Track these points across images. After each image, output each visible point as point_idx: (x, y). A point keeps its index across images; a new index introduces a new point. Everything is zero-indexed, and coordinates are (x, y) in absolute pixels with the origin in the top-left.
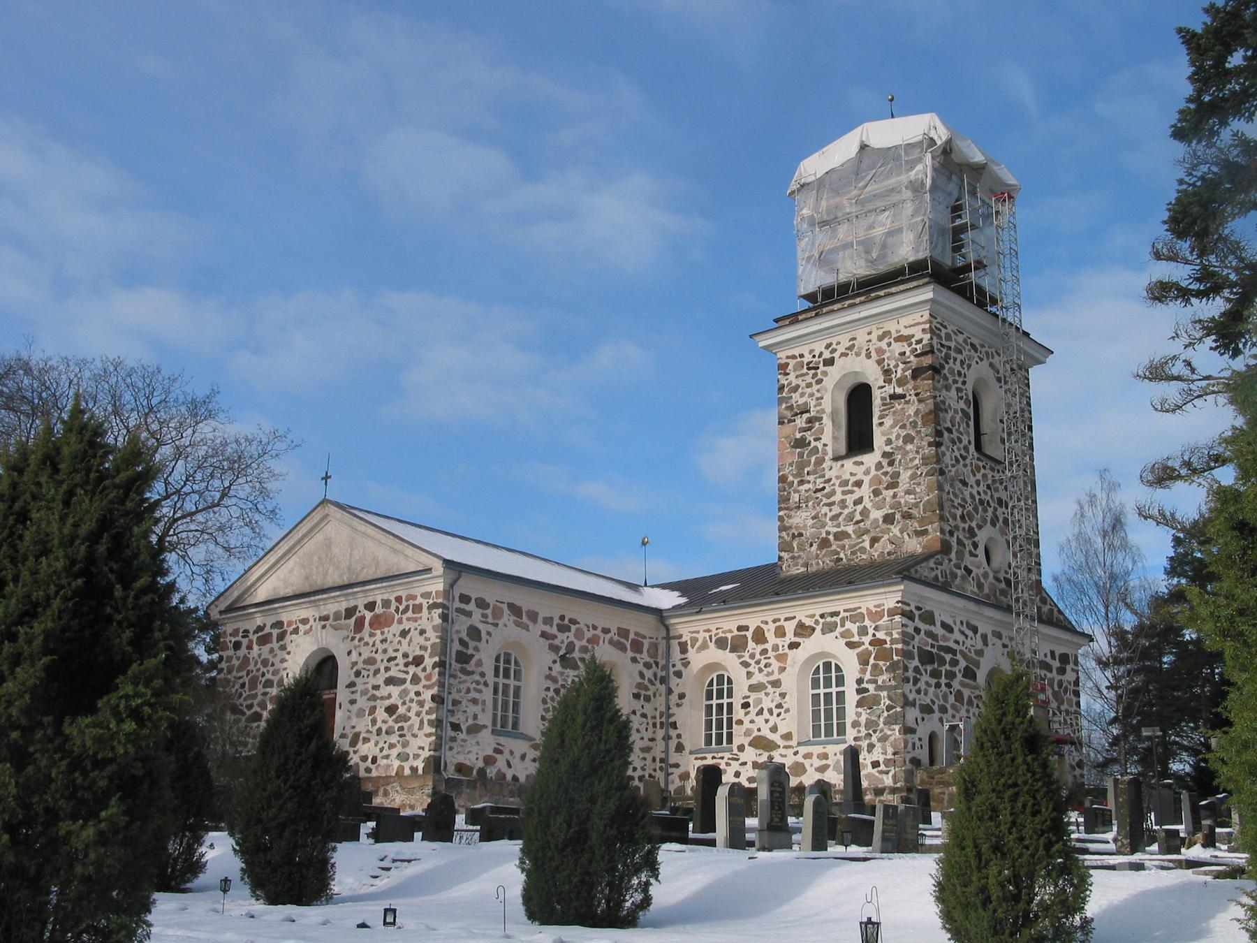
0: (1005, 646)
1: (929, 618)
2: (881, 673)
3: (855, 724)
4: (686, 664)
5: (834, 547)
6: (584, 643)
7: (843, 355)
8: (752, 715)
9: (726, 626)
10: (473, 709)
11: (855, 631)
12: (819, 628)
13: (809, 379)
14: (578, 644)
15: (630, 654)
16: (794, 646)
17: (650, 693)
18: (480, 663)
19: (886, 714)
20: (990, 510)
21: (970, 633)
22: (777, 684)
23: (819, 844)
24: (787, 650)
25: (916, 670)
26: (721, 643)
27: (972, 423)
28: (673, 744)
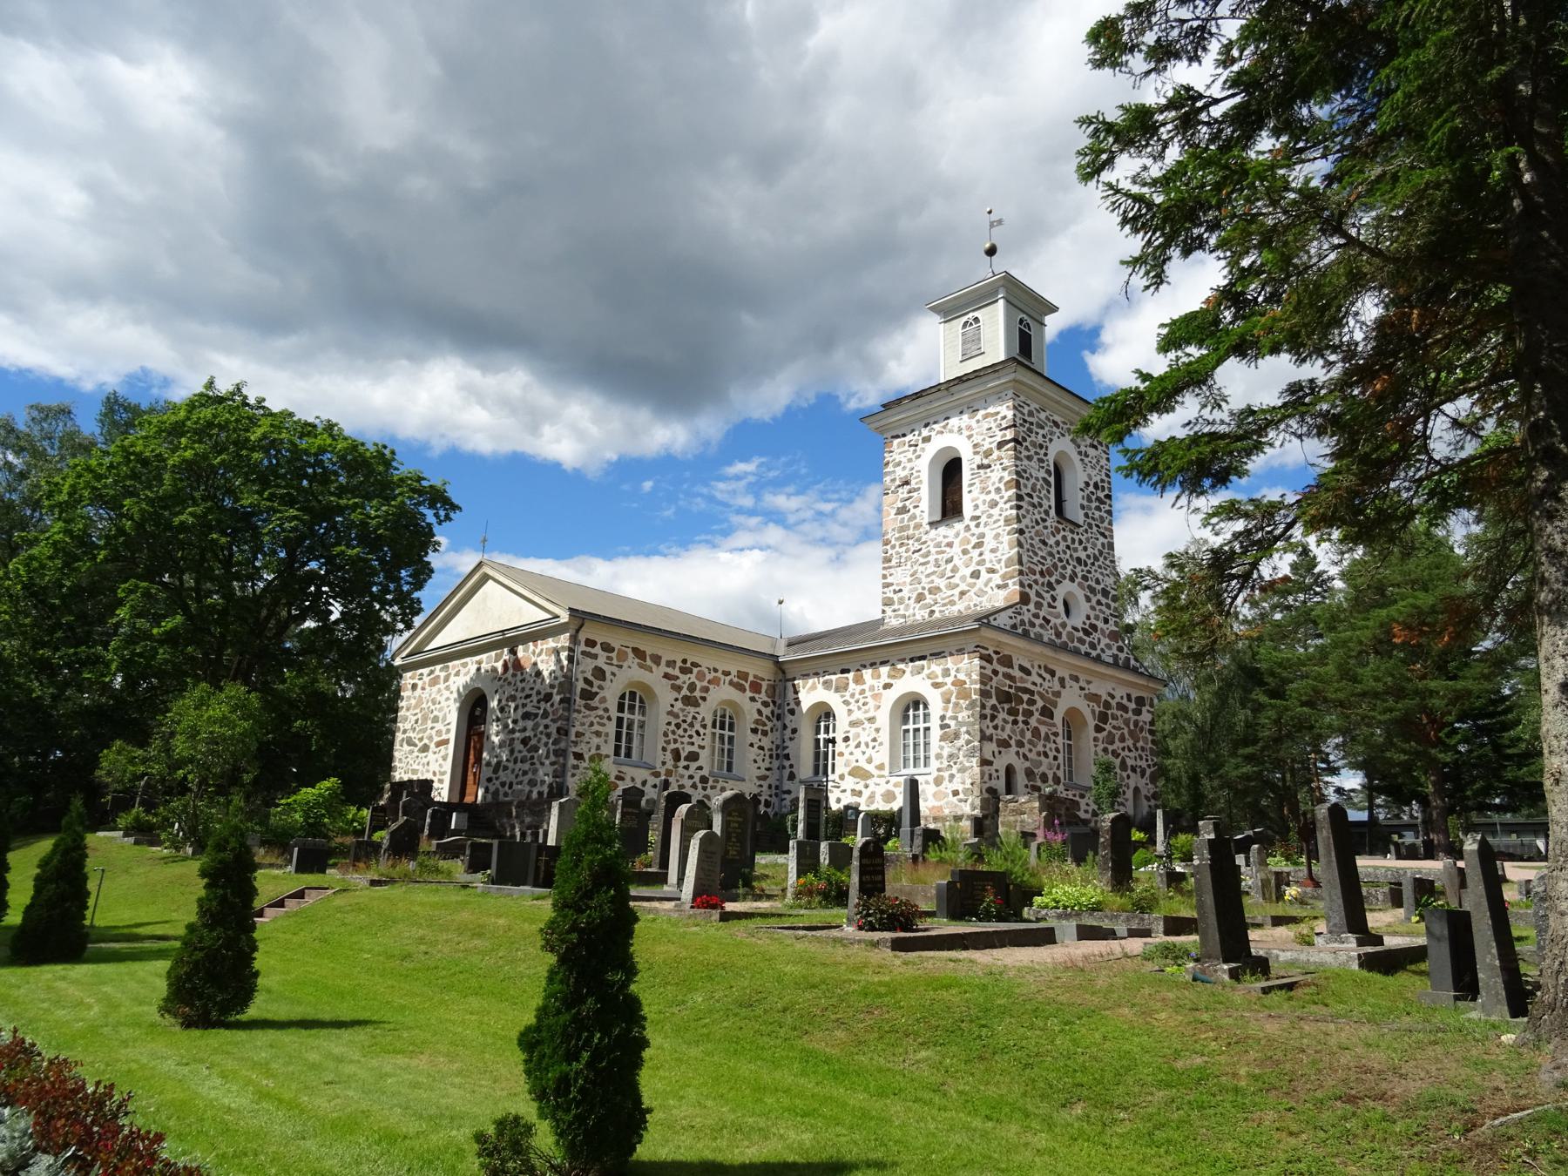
0: (1082, 689)
1: (1007, 661)
3: (939, 756)
4: (798, 703)
6: (705, 683)
8: (852, 748)
10: (596, 740)
11: (939, 673)
13: (910, 455)
14: (699, 685)
15: (749, 694)
16: (887, 686)
17: (767, 728)
18: (603, 700)
20: (1069, 568)
21: (1048, 676)
22: (871, 720)
23: (298, 870)
25: (994, 707)
27: (1052, 490)
28: (786, 773)
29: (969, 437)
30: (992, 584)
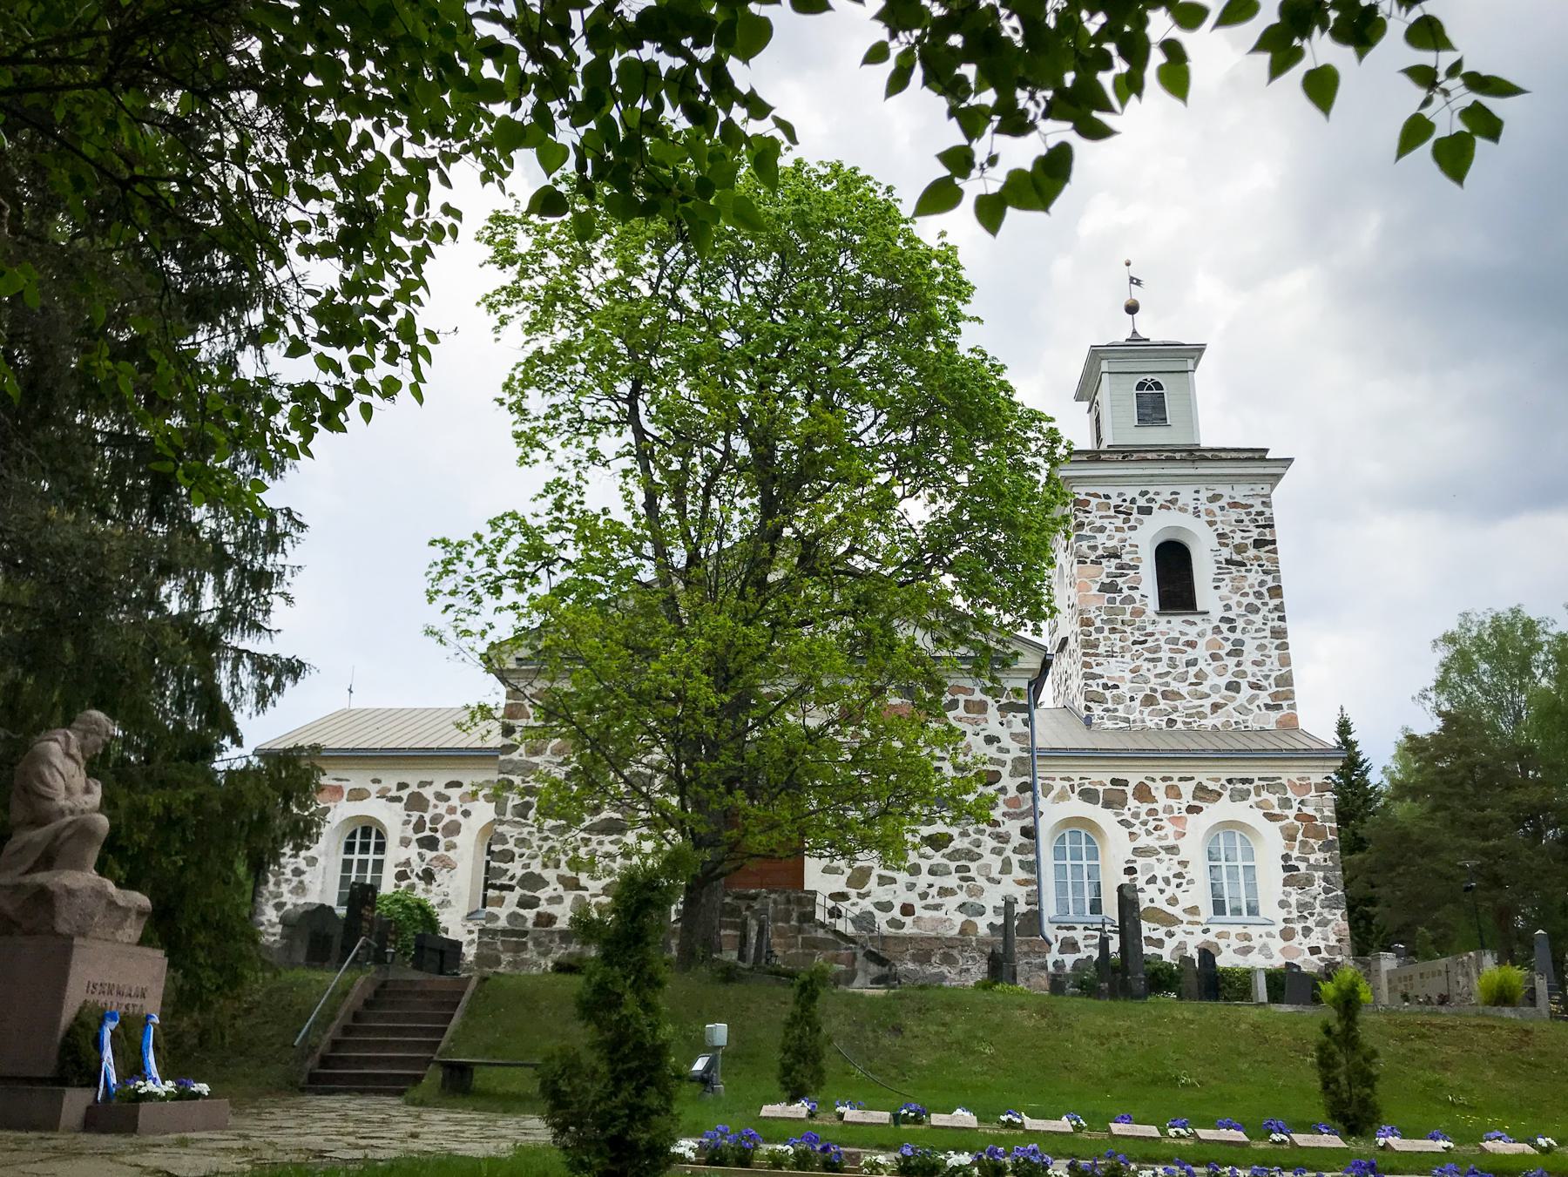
2: (1313, 851)
5: (1162, 706)
7: (1161, 507)
9: (1095, 777)
12: (1226, 794)
19: (1323, 896)
22: (1172, 850)
24: (1184, 814)
26: (1088, 795)
29: (1211, 524)
30: (1260, 702)
